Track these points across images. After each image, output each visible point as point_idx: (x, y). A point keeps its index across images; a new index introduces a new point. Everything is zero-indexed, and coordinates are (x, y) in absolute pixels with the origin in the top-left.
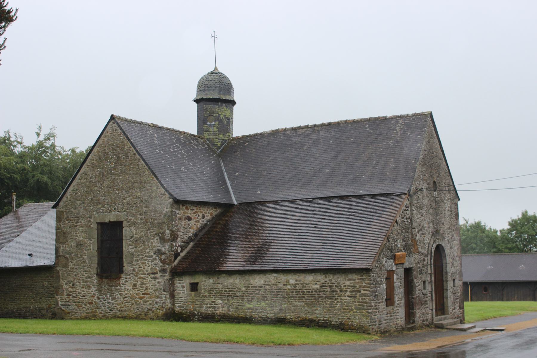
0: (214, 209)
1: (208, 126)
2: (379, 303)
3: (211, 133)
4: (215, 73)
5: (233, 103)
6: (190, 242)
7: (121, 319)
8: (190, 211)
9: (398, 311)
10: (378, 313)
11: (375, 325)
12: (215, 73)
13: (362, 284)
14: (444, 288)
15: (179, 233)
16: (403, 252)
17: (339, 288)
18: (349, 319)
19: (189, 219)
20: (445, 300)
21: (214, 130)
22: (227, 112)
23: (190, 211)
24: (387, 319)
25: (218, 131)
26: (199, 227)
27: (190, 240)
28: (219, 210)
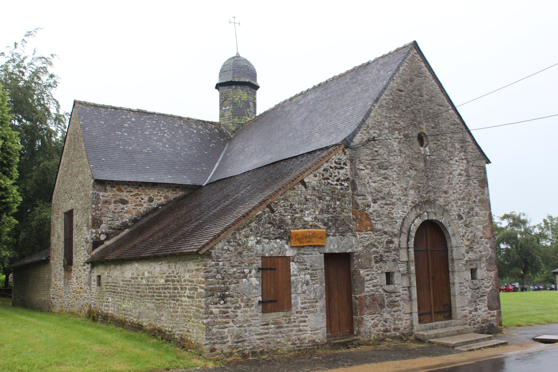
0: (171, 192)
1: (223, 111)
3: (226, 118)
4: (238, 57)
5: (256, 87)
6: (125, 229)
8: (125, 193)
12: (238, 57)
13: (199, 277)
14: (450, 281)
15: (103, 218)
16: (320, 228)
17: (180, 283)
18: (188, 331)
19: (124, 202)
20: (452, 298)
21: (229, 115)
22: (243, 95)
23: (125, 193)
24: (268, 333)
25: (232, 115)
26: (142, 212)
27: (125, 226)
28: (180, 193)
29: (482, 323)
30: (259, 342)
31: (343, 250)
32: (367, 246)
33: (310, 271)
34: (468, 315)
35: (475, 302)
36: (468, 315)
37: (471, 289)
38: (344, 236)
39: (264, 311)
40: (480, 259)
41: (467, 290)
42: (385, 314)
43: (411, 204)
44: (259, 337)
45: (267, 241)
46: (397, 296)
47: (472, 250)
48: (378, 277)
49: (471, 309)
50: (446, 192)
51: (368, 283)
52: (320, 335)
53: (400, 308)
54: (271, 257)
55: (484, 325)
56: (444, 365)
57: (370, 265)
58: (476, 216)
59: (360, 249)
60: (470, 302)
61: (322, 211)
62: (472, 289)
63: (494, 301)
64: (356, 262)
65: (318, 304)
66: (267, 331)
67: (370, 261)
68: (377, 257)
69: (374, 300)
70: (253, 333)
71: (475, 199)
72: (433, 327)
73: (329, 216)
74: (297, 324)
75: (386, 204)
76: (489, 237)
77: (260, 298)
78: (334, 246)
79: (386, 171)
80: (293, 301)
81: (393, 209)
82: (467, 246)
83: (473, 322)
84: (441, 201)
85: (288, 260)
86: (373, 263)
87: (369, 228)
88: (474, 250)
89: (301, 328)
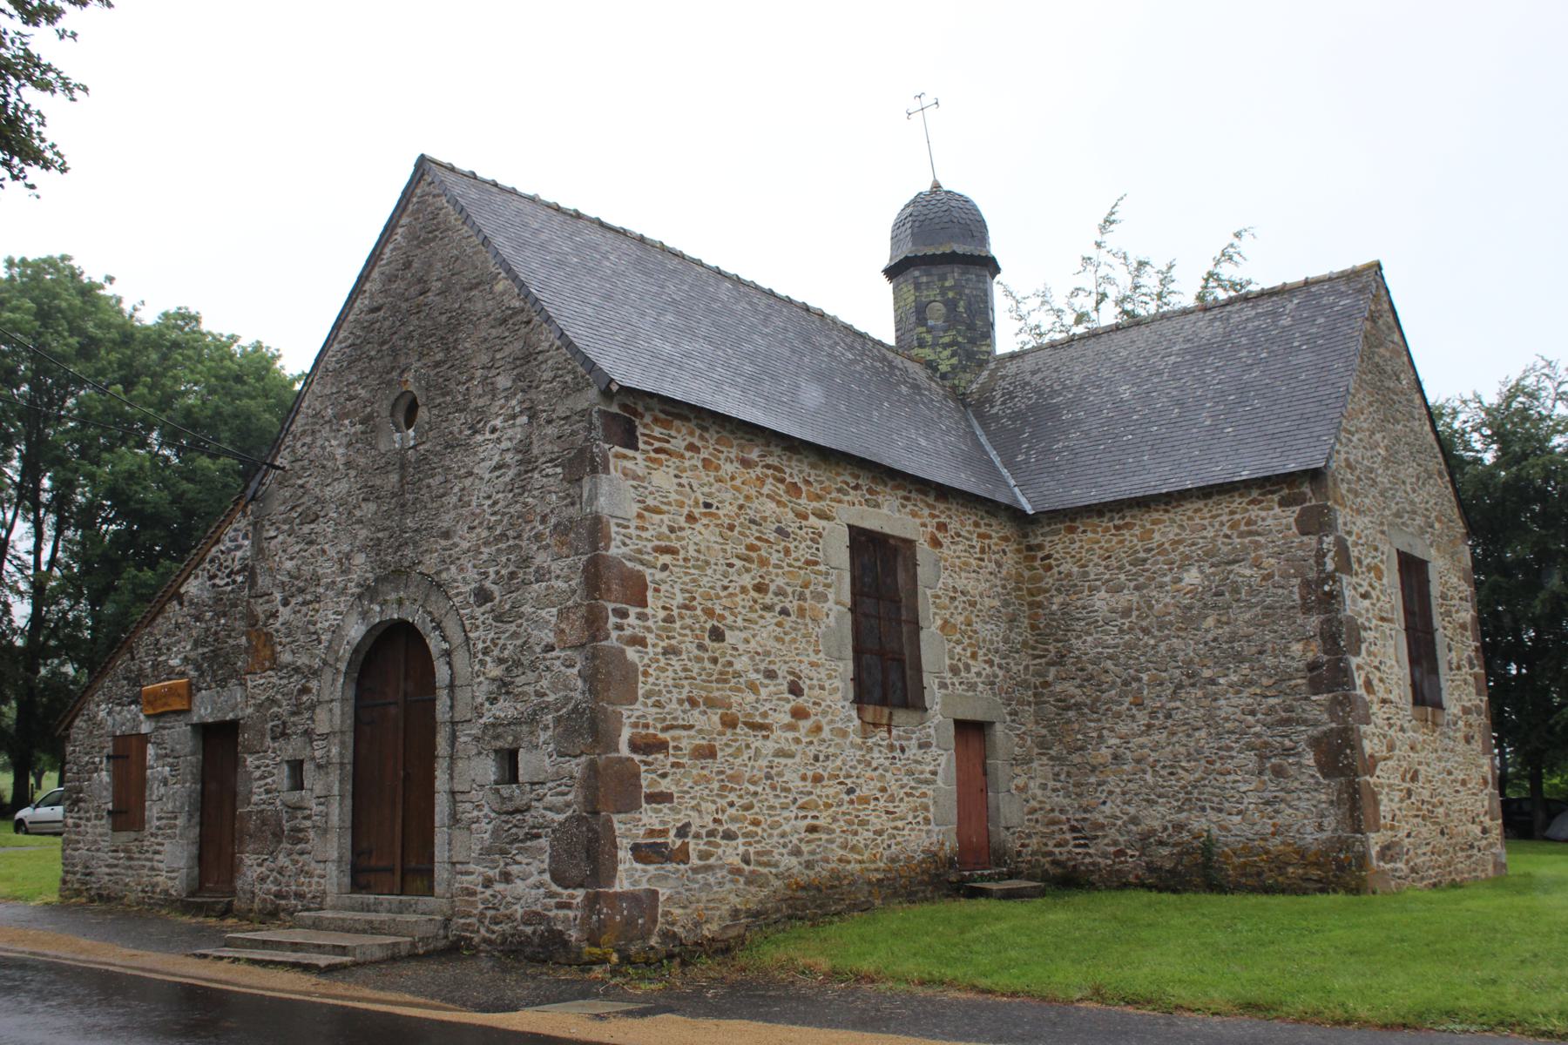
2: (88, 819)
7: (1039, 901)
9: (158, 848)
10: (81, 845)
11: (75, 873)
24: (116, 866)
29: (525, 924)
30: (107, 878)
31: (219, 717)
32: (261, 705)
33: (170, 760)
34: (479, 889)
35: (503, 852)
36: (479, 889)
37: (494, 811)
38: (222, 687)
39: (116, 828)
40: (532, 720)
41: (481, 814)
42: (281, 857)
43: (354, 590)
44: (107, 870)
45: (118, 708)
46: (305, 818)
47: (508, 693)
48: (275, 771)
49: (491, 873)
50: (446, 535)
51: (256, 784)
52: (177, 882)
53: (308, 847)
54: (123, 736)
55: (529, 930)
56: (156, 972)
57: (262, 744)
58: (537, 581)
59: (250, 710)
60: (487, 851)
61: (196, 644)
62: (499, 813)
63: (572, 856)
64: (245, 737)
65: (177, 822)
66: (116, 862)
67: (263, 735)
68: (277, 726)
69: (264, 823)
70: (101, 863)
71: (541, 527)
72: (368, 905)
73: (206, 650)
74: (149, 855)
75: (305, 603)
76: (576, 642)
77: (110, 806)
78: (206, 709)
79: (312, 526)
80: (147, 813)
81: (317, 611)
82: (494, 680)
83: (490, 913)
84: (430, 563)
85: (144, 739)
86: (268, 741)
87: (267, 664)
88: (516, 691)
89: (155, 864)
